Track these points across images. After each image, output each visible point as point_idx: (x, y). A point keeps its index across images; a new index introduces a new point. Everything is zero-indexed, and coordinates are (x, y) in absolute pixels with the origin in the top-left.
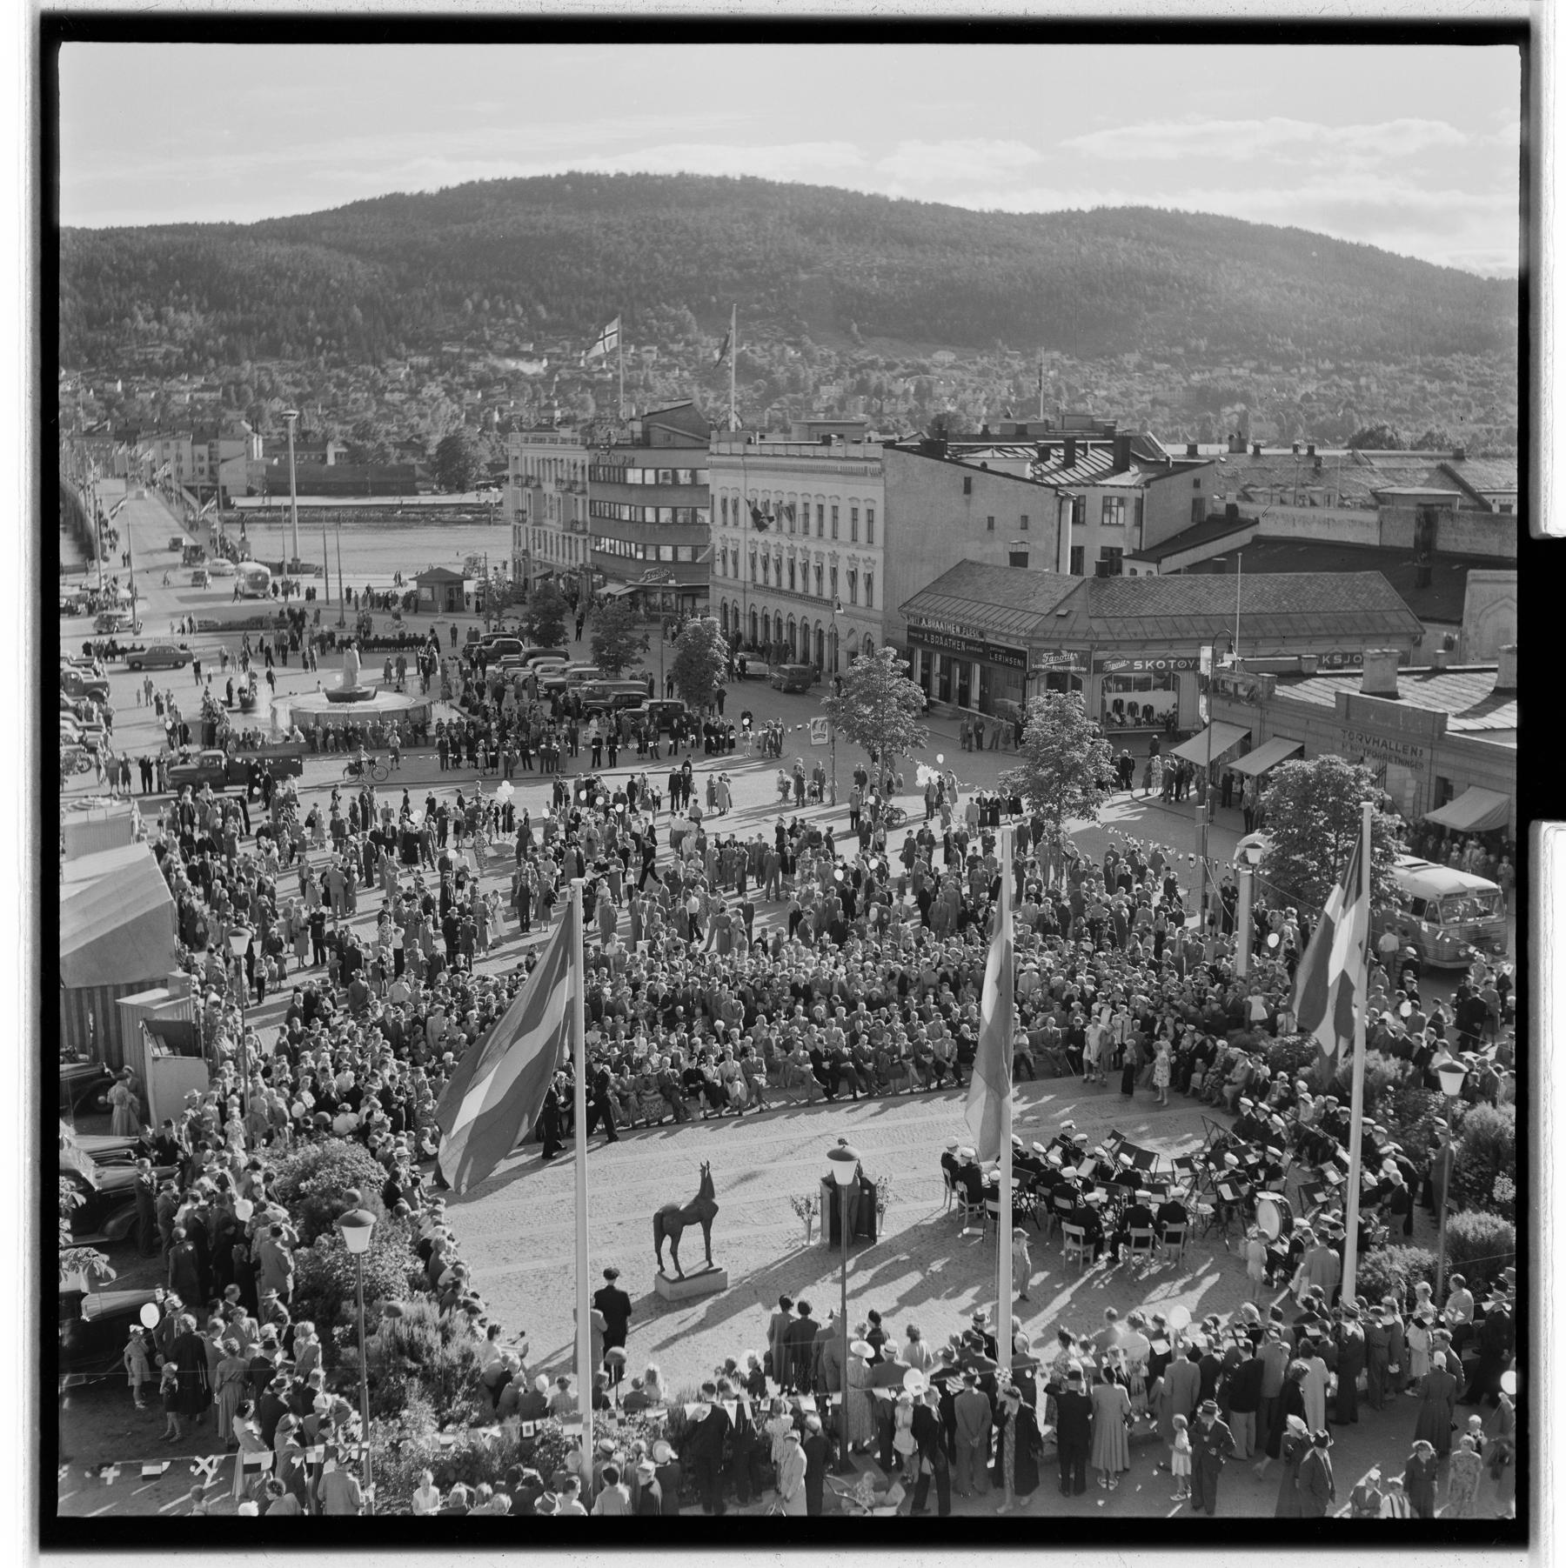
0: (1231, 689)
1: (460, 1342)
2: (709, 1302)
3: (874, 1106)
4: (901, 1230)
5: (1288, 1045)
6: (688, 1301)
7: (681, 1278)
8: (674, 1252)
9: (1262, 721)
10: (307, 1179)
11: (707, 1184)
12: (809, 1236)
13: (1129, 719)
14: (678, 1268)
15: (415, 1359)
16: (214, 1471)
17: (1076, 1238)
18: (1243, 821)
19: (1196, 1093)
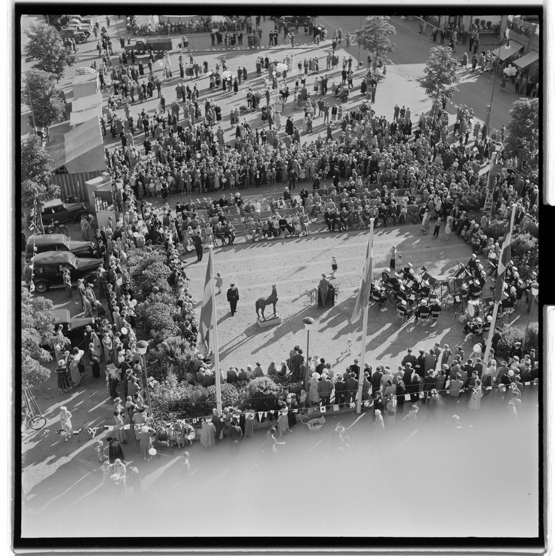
0: (519, 28)
1: (187, 351)
2: (274, 329)
3: (345, 235)
4: (344, 300)
5: (497, 225)
6: (267, 328)
7: (265, 321)
8: (262, 313)
9: (529, 43)
10: (144, 270)
11: (274, 293)
12: (311, 302)
13: (481, 27)
14: (264, 317)
15: (172, 357)
16: (95, 432)
17: (401, 314)
18: (515, 87)
19: (462, 237)
